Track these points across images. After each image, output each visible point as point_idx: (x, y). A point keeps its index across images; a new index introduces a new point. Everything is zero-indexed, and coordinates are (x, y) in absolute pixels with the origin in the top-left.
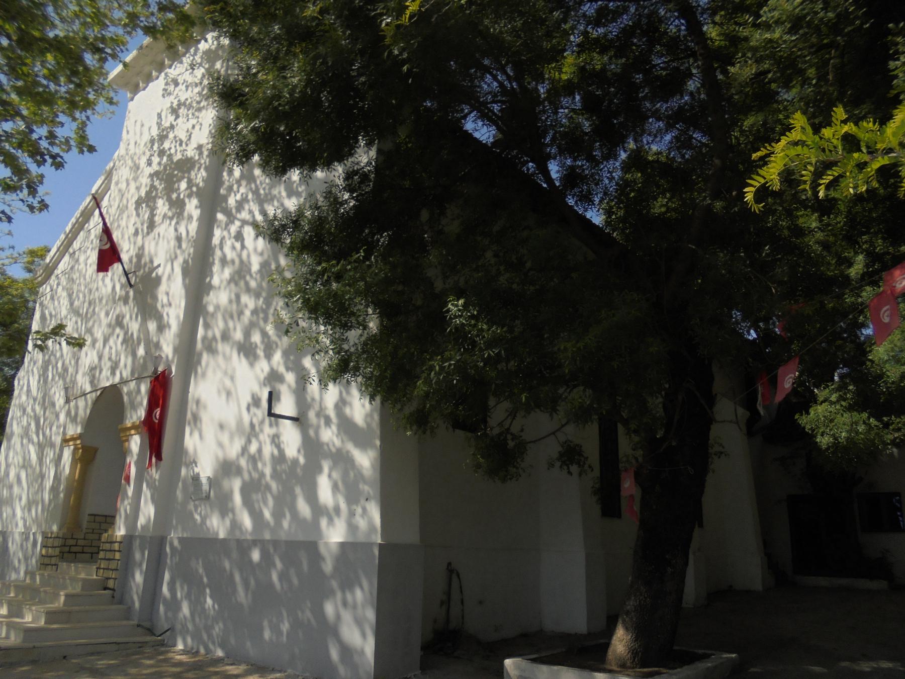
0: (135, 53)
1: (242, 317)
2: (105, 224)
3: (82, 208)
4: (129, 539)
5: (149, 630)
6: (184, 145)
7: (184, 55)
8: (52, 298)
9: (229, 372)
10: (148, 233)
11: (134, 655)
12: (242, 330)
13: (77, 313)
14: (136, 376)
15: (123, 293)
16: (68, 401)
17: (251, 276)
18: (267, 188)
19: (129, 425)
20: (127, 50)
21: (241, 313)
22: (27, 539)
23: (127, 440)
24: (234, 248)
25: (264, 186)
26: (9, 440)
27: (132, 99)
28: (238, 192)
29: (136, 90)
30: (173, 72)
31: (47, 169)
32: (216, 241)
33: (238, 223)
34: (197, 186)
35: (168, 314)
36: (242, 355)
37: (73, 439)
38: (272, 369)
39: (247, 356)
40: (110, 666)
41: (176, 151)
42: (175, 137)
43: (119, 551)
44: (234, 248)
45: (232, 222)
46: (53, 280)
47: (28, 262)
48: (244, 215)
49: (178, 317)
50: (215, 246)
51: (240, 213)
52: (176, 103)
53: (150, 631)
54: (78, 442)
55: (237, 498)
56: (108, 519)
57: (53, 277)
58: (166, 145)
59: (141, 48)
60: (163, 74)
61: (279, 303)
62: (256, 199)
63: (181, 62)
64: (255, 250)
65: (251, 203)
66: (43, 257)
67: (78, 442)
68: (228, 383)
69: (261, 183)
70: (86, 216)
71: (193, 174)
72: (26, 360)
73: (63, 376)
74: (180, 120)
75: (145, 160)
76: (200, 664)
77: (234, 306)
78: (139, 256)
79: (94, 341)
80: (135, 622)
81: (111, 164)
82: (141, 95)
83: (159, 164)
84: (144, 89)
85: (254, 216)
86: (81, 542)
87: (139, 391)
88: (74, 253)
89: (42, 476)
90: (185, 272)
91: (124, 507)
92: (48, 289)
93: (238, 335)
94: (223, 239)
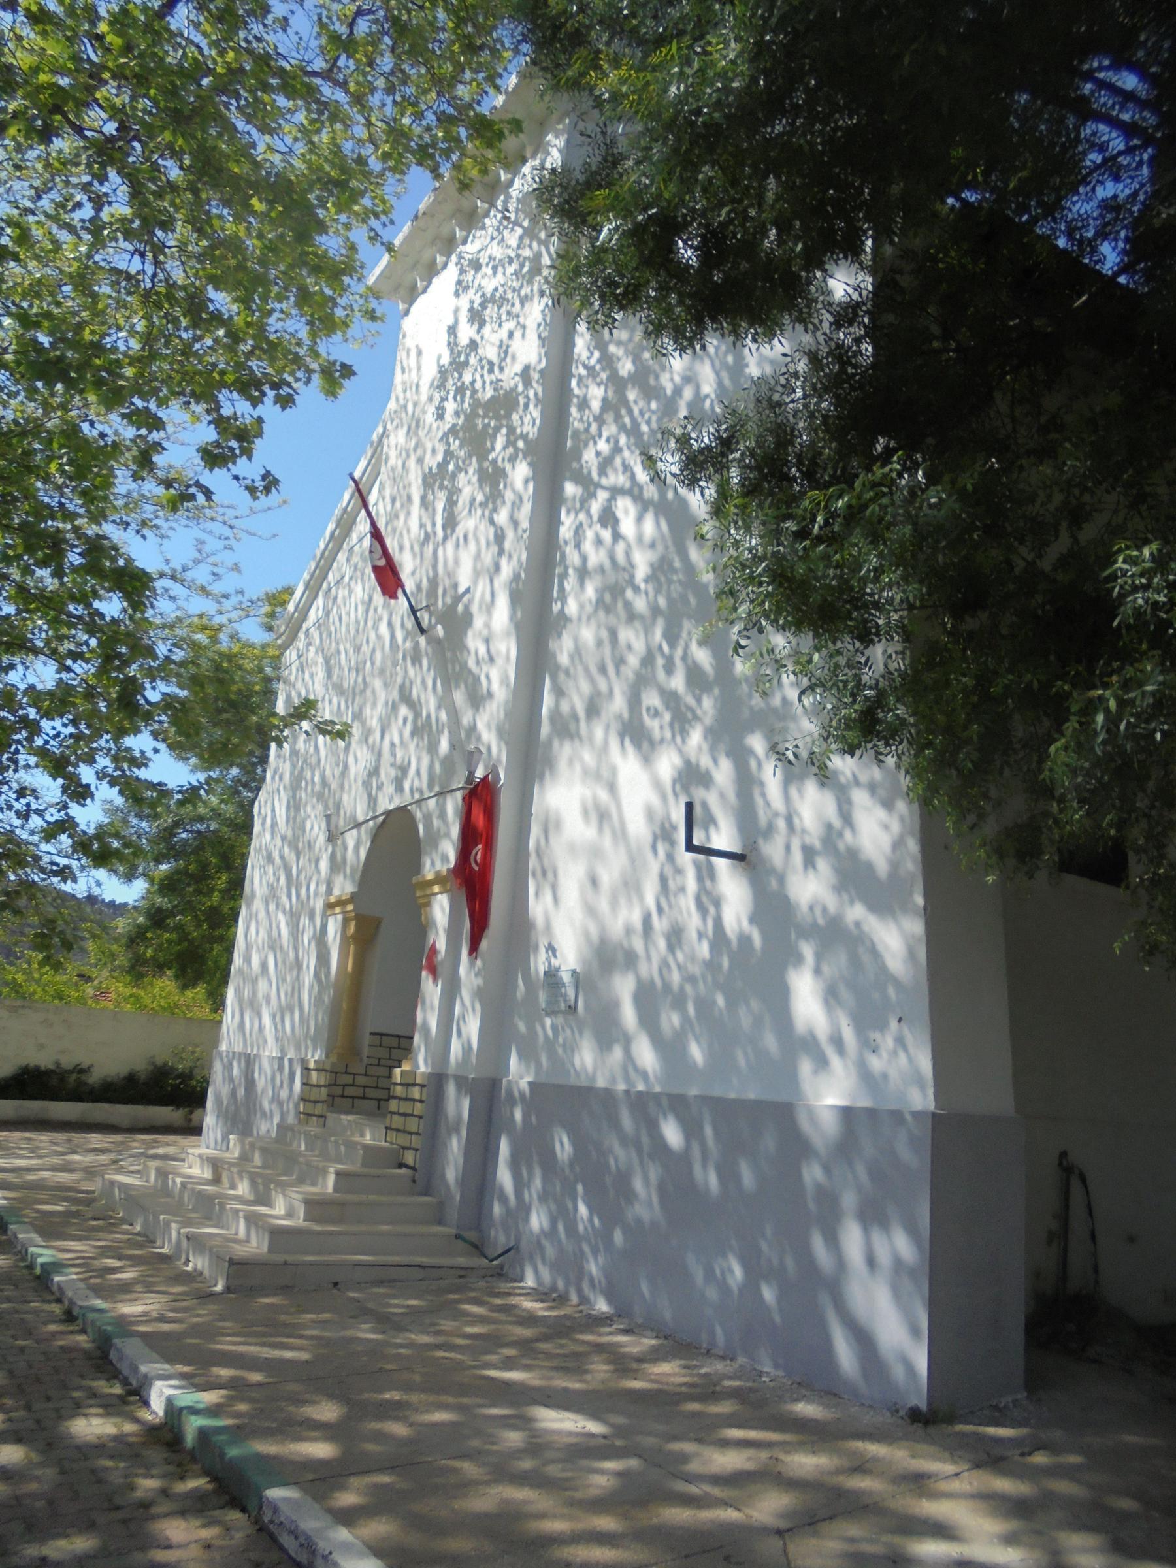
0: (406, 229)
1: (623, 668)
2: (373, 524)
3: (337, 512)
4: (438, 1080)
5: (476, 1247)
6: (496, 370)
7: (487, 215)
8: (302, 668)
9: (605, 773)
10: (445, 538)
11: (452, 1292)
12: (624, 693)
13: (340, 690)
14: (437, 789)
15: (408, 645)
16: (331, 839)
17: (636, 589)
18: (654, 418)
19: (430, 876)
20: (392, 222)
21: (620, 662)
22: (281, 1068)
23: (428, 904)
24: (599, 541)
25: (647, 416)
26: (249, 906)
27: (407, 313)
28: (600, 436)
29: (412, 295)
30: (471, 248)
31: (268, 409)
32: (565, 531)
33: (602, 495)
34: (524, 437)
35: (488, 677)
36: (627, 741)
37: (340, 903)
38: (688, 763)
39: (638, 745)
40: (414, 1312)
41: (484, 383)
42: (481, 360)
43: (421, 1101)
44: (599, 541)
45: (593, 495)
46: (301, 643)
47: (266, 615)
48: (617, 478)
49: (504, 680)
50: (566, 543)
51: (606, 475)
52: (478, 300)
53: (478, 1248)
54: (350, 907)
55: (629, 1015)
56: (403, 1042)
57: (301, 635)
58: (467, 378)
59: (416, 217)
60: (454, 258)
61: (691, 631)
62: (636, 445)
63: (484, 228)
64: (640, 538)
65: (626, 453)
66: (283, 604)
67: (350, 907)
68: (603, 795)
69: (642, 413)
70: (346, 525)
71: (515, 417)
72: (269, 775)
73: (320, 797)
74: (487, 330)
75: (431, 409)
76: (568, 1323)
77: (607, 650)
78: (434, 582)
79: (367, 733)
80: (453, 1231)
81: (380, 429)
82: (421, 303)
83: (457, 414)
84: (424, 291)
85: (633, 477)
86: (361, 1080)
87: (442, 815)
88: (330, 589)
89: (298, 964)
90: (515, 598)
91: (429, 1017)
92: (294, 656)
93: (619, 704)
94: (578, 530)
